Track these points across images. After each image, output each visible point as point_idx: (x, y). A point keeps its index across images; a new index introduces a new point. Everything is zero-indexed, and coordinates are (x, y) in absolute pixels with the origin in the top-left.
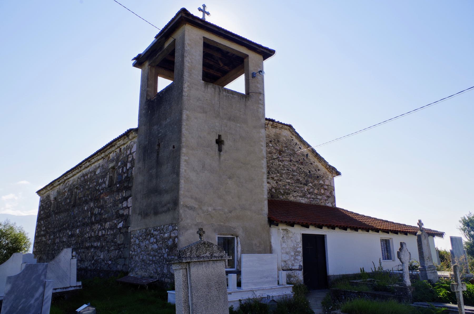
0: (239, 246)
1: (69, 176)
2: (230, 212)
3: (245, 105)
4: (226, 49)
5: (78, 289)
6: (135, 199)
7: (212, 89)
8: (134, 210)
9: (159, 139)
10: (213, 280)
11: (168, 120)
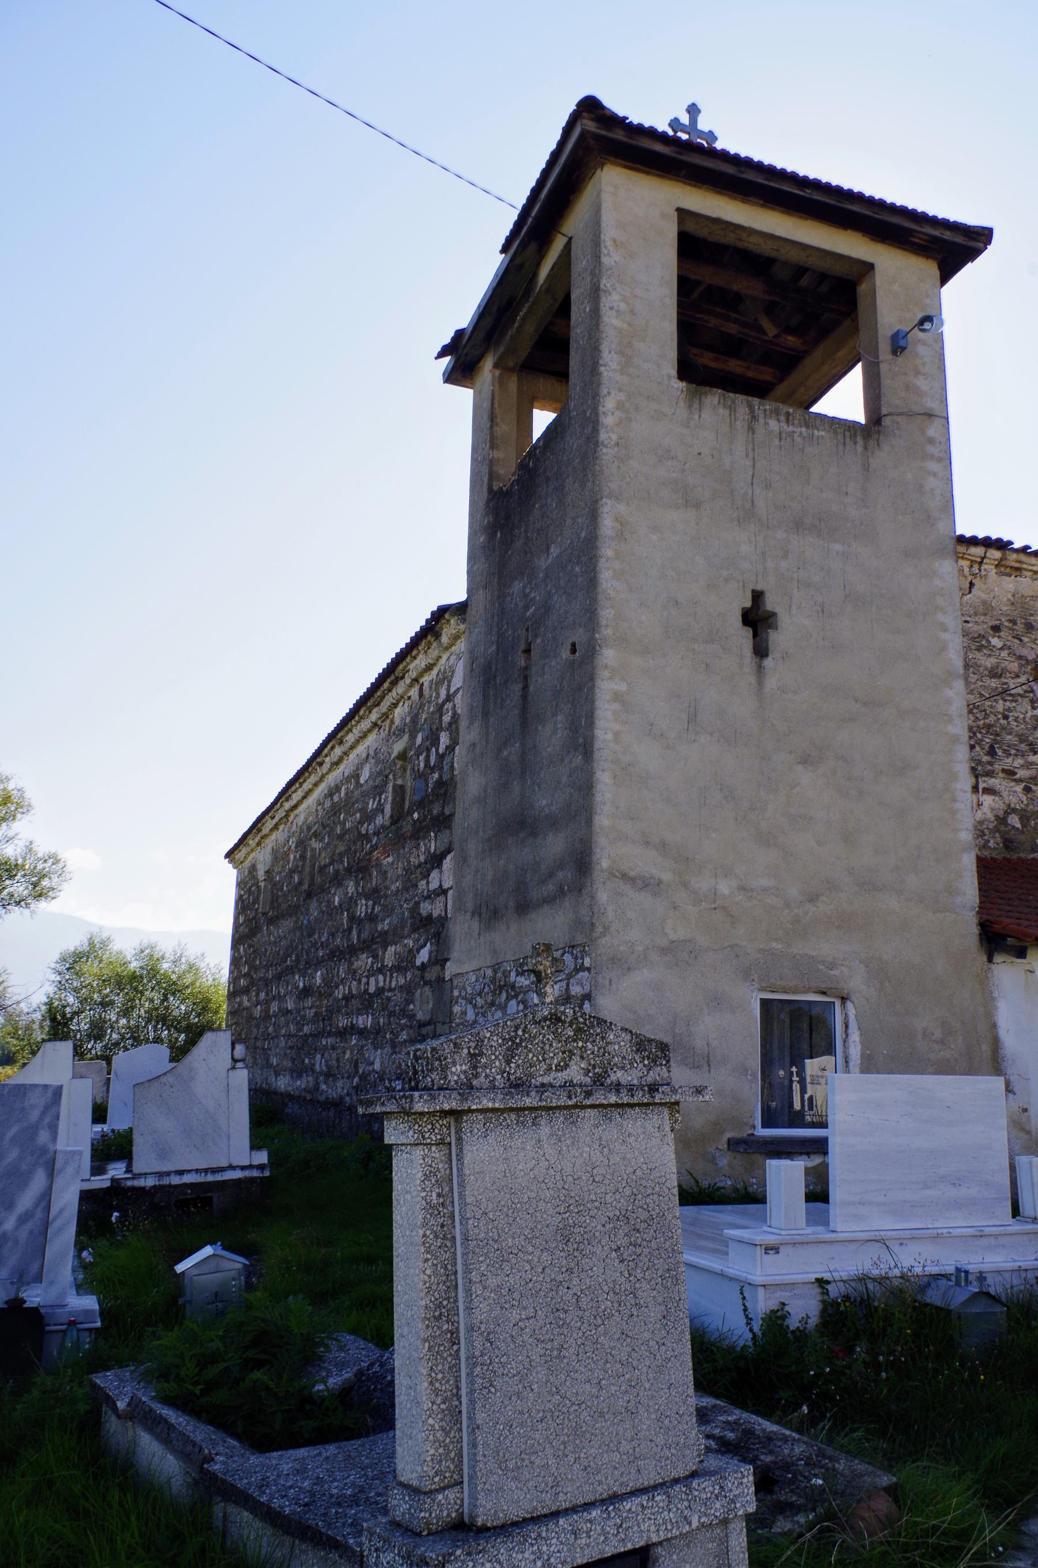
0: (855, 1037)
1: (296, 797)
2: (811, 900)
3: (866, 467)
4: (777, 250)
5: (256, 1177)
6: (463, 860)
7: (721, 411)
8: (459, 899)
9: (527, 630)
10: (597, 1204)
11: (554, 551)
